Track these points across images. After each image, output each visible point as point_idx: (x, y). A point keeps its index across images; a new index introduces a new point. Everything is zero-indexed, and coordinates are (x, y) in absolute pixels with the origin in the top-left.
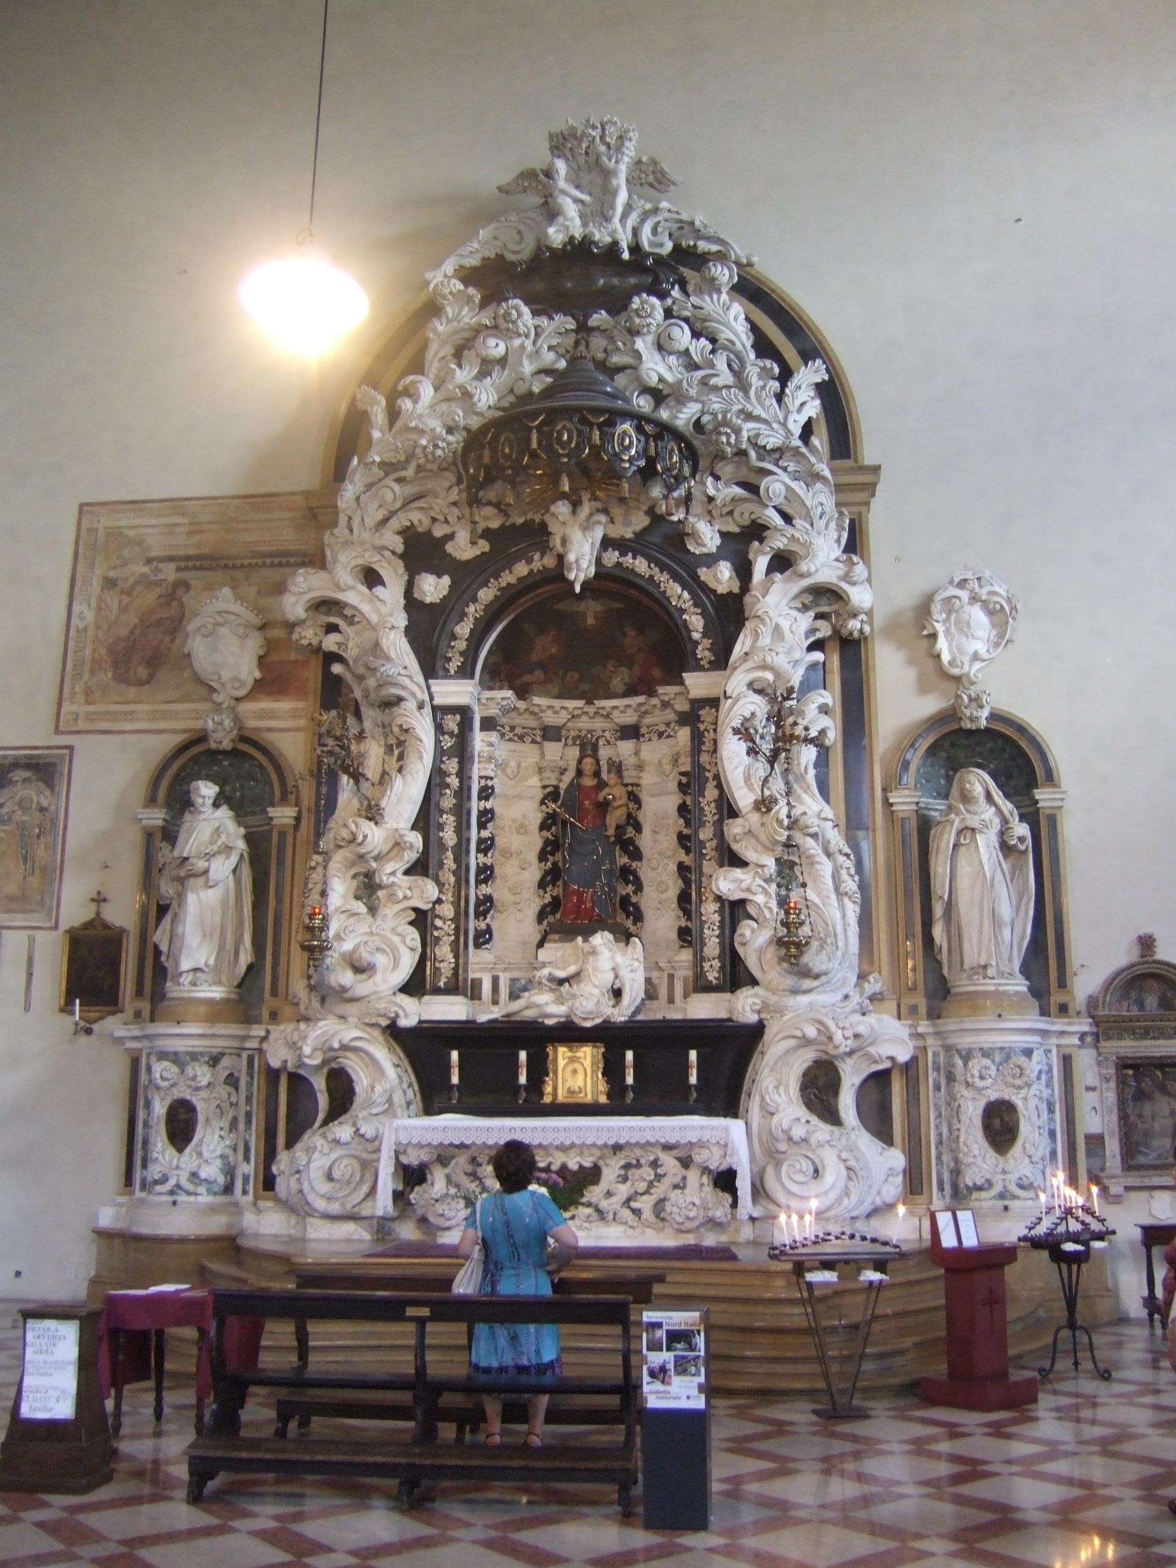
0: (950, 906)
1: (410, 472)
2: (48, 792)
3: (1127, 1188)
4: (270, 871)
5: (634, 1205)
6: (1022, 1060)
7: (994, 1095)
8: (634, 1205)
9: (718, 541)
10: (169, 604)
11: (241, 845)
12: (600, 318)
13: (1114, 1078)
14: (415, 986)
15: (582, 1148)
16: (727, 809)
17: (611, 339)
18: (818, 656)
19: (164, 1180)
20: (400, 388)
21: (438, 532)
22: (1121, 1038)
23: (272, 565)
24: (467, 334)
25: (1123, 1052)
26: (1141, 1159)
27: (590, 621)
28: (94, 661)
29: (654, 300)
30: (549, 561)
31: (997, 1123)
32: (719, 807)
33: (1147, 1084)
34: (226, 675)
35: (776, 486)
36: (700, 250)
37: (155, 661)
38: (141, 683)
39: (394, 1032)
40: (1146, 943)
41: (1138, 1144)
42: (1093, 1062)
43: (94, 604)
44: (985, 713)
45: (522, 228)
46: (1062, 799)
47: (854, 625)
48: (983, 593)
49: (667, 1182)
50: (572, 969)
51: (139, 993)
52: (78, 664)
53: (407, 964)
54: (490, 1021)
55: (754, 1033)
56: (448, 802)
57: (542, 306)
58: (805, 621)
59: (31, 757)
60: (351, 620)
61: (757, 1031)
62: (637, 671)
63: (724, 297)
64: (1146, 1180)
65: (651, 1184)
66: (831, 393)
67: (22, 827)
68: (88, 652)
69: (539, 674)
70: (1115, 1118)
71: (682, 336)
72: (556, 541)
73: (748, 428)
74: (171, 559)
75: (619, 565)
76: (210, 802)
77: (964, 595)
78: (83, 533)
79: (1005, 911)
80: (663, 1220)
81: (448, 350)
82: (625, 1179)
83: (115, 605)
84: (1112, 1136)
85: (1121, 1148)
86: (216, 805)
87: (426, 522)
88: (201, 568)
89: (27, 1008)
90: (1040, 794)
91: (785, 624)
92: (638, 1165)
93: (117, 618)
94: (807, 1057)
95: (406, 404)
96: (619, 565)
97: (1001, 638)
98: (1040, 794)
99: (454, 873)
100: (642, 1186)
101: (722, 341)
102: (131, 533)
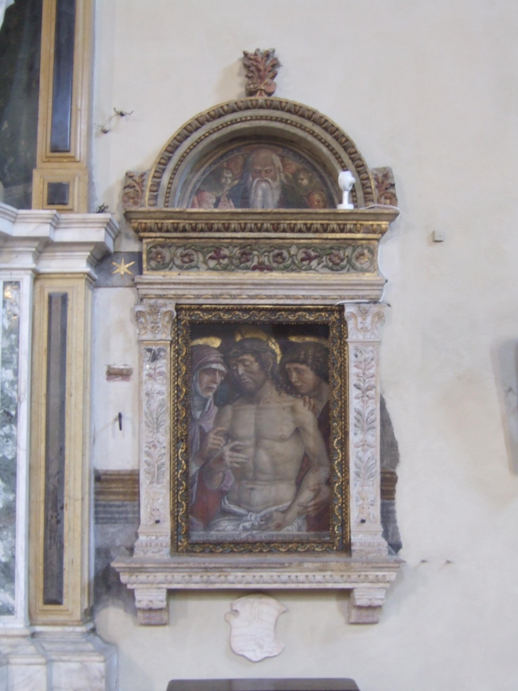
3: (172, 593)
13: (168, 352)
22: (187, 264)
25: (190, 296)
26: (226, 529)
33: (248, 368)
40: (260, 68)
41: (222, 493)
42: (127, 315)
46: (381, 290)
64: (214, 576)
70: (164, 438)
84: (155, 479)
85: (176, 505)
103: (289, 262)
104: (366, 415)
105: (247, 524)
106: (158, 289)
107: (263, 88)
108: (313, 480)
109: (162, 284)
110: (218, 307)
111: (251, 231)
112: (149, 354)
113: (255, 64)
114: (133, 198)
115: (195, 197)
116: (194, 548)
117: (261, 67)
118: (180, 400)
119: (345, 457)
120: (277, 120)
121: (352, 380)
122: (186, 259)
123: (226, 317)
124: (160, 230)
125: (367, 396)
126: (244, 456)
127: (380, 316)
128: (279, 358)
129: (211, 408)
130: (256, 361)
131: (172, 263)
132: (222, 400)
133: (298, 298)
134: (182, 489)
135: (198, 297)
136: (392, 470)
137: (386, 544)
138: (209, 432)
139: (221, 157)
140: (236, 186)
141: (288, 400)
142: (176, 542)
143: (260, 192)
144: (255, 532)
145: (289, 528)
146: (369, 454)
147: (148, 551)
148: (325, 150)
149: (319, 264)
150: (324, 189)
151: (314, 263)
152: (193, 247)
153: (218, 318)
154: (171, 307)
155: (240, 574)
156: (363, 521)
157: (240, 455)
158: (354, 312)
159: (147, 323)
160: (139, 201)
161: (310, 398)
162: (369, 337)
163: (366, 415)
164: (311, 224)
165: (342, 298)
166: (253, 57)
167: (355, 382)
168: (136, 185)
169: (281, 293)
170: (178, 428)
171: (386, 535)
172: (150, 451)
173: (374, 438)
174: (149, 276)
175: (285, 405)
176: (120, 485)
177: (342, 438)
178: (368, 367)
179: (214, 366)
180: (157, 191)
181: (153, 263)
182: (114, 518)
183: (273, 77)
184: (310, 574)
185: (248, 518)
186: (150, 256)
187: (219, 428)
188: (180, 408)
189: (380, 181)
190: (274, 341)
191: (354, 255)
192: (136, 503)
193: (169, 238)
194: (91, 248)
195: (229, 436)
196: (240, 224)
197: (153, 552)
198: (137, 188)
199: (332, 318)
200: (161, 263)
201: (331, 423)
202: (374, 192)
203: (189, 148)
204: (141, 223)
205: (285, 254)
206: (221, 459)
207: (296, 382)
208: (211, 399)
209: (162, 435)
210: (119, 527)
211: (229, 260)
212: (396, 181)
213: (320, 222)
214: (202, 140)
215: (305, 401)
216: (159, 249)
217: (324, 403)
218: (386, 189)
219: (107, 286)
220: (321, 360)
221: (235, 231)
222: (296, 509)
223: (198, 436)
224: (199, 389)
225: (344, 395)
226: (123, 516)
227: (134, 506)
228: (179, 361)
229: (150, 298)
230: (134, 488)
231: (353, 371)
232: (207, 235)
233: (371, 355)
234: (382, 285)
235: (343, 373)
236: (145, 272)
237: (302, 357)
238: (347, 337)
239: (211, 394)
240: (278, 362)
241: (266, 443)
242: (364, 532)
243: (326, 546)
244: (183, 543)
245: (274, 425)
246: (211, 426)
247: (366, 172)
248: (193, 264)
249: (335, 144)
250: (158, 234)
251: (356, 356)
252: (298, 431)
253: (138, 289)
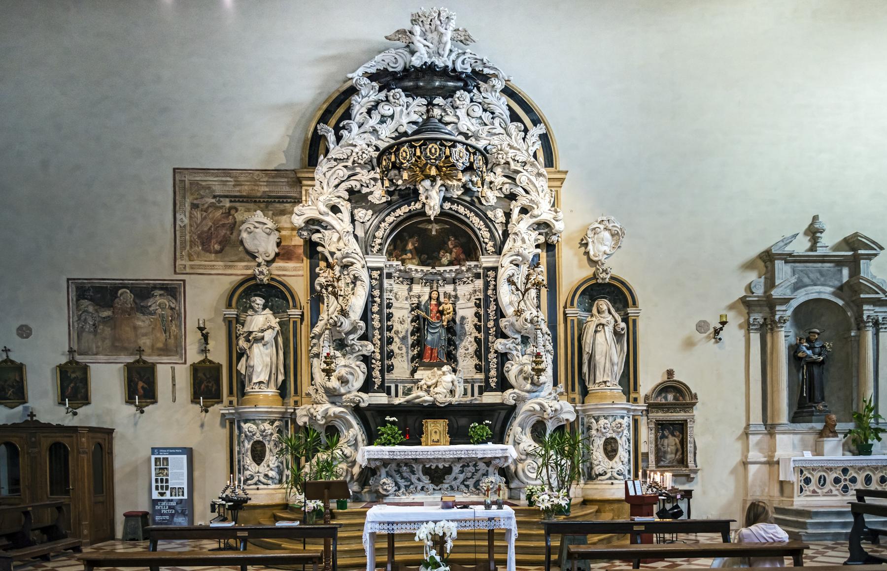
0: (591, 357)
1: (349, 164)
2: (174, 301)
4: (288, 339)
5: (466, 483)
6: (620, 420)
7: (609, 436)
8: (466, 483)
9: (495, 200)
10: (228, 217)
11: (278, 328)
12: (439, 100)
14: (367, 387)
15: (445, 460)
16: (500, 314)
17: (445, 110)
18: (539, 251)
19: (252, 477)
20: (341, 125)
21: (365, 190)
23: (279, 202)
24: (373, 104)
27: (434, 233)
28: (191, 241)
29: (466, 93)
30: (418, 206)
31: (609, 448)
32: (496, 314)
34: (261, 250)
35: (522, 178)
36: (485, 73)
37: (225, 243)
38: (217, 252)
39: (357, 410)
40: (670, 373)
43: (187, 214)
44: (609, 276)
45: (397, 56)
47: (554, 238)
48: (610, 226)
49: (480, 473)
50: (434, 381)
51: (231, 393)
52: (183, 243)
53: (362, 378)
54: (400, 404)
55: (510, 411)
56: (376, 308)
57: (411, 92)
58: (535, 234)
59: (163, 284)
60: (325, 228)
61: (513, 408)
62: (454, 255)
63: (498, 94)
65: (473, 474)
66: (545, 139)
67: (162, 316)
68: (188, 237)
69: (409, 255)
70: (653, 446)
71: (478, 111)
72: (422, 198)
73: (511, 153)
74: (226, 197)
75: (451, 209)
76: (261, 307)
77: (602, 227)
78: (177, 182)
79: (615, 359)
80: (478, 489)
81: (364, 110)
82: (462, 472)
83: (199, 216)
86: (264, 309)
87: (359, 186)
88: (243, 202)
89: (174, 400)
90: (630, 310)
91: (526, 238)
92: (468, 466)
93: (202, 222)
94: (534, 419)
95: (344, 133)
96: (451, 209)
97: (617, 246)
98: (630, 310)
99: (380, 340)
100: (469, 475)
101: (497, 114)
102: (204, 183)
108: (679, 453)
173: (692, 445)
242: (691, 464)
245: (671, 443)
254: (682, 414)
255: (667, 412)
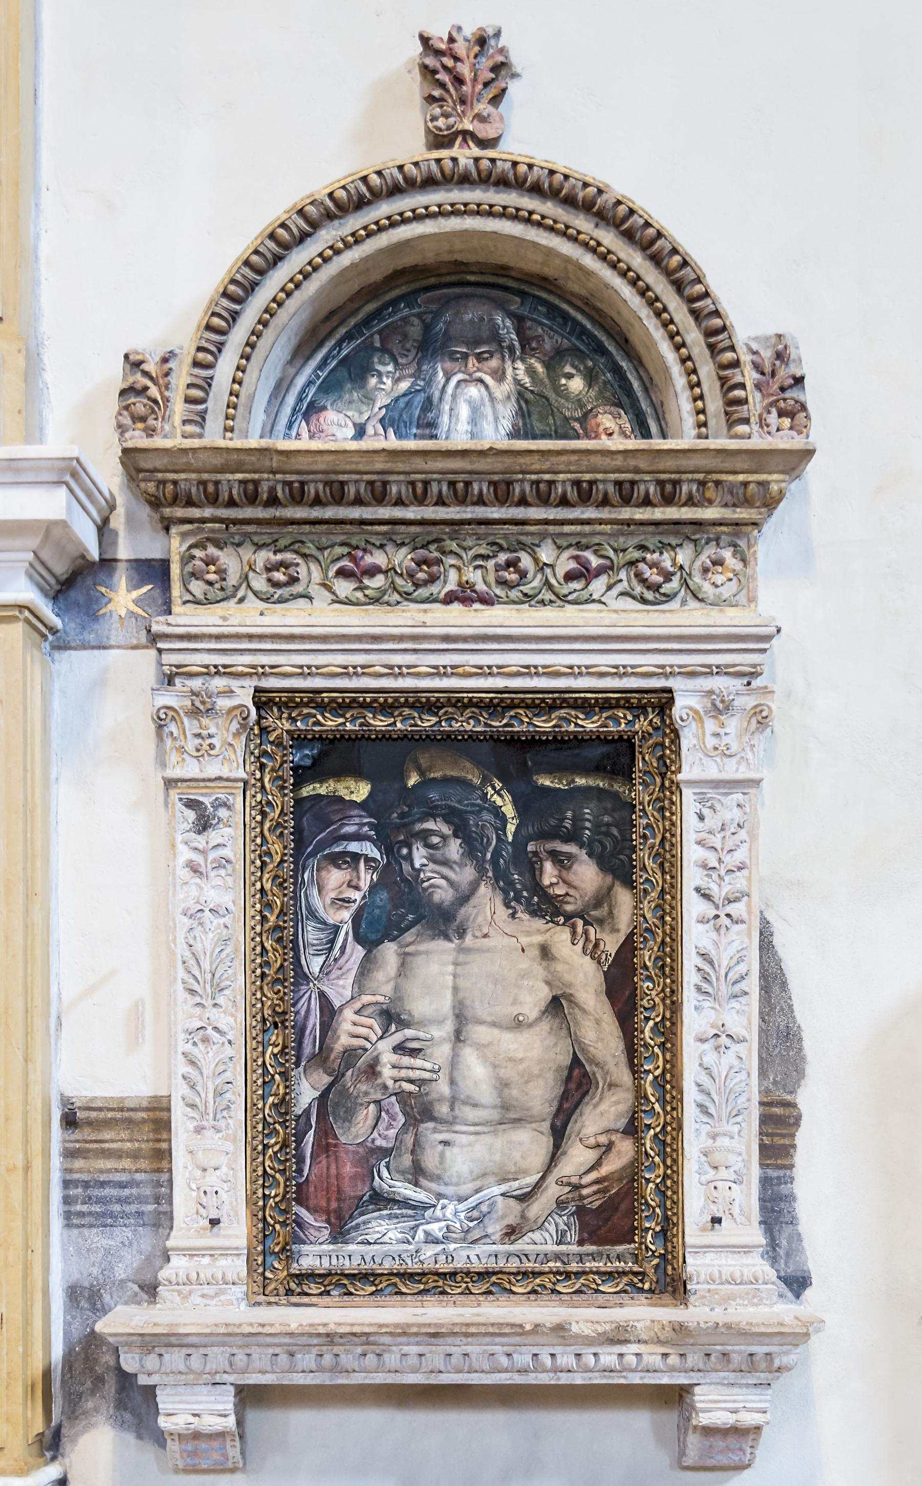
3: (250, 1397)
25: (291, 670)
40: (460, 74)
70: (231, 1017)
103: (536, 583)
104: (724, 964)
105: (436, 1228)
106: (209, 651)
107: (470, 128)
108: (601, 1115)
109: (218, 637)
110: (361, 697)
111: (441, 502)
112: (191, 815)
113: (449, 63)
114: (143, 419)
115: (303, 423)
116: (303, 1284)
117: (465, 70)
118: (267, 926)
119: (673, 1066)
120: (504, 214)
121: (692, 877)
122: (279, 576)
123: (380, 723)
124: (213, 500)
125: (728, 915)
126: (428, 1065)
127: (761, 719)
128: (511, 828)
129: (348, 950)
130: (456, 836)
131: (244, 585)
132: (373, 930)
133: (558, 675)
134: (276, 1143)
135: (305, 672)
136: (788, 1097)
137: (772, 1274)
138: (342, 1008)
139: (366, 322)
140: (404, 395)
141: (534, 930)
142: (261, 1270)
143: (464, 411)
144: (452, 1246)
145: (536, 1236)
146: (729, 1058)
147: (190, 1293)
148: (627, 291)
149: (610, 588)
150: (625, 400)
151: (598, 586)
152: (296, 546)
153: (361, 725)
154: (245, 697)
155: (414, 1350)
156: (716, 1221)
157: (418, 1063)
158: (699, 707)
159: (186, 737)
160: (158, 424)
161: (586, 923)
162: (732, 770)
163: (724, 964)
164: (591, 483)
165: (664, 672)
166: (443, 46)
167: (698, 882)
168: (149, 383)
169: (515, 660)
170: (263, 995)
171: (772, 1251)
172: (195, 1051)
173: (744, 1018)
174: (186, 617)
175: (524, 940)
176: (124, 1135)
177: (664, 1017)
178: (729, 844)
179: (354, 847)
180: (203, 401)
181: (197, 587)
182: (112, 1215)
183: (496, 100)
184: (588, 1351)
185: (438, 1213)
186: (189, 568)
187: (366, 999)
188: (268, 945)
189: (768, 369)
190: (498, 785)
191: (698, 564)
192: (165, 1177)
193: (235, 522)
194: (34, 542)
195: (391, 1017)
196: (413, 483)
197: (203, 1296)
198: (154, 391)
199: (641, 725)
200: (217, 586)
201: (639, 985)
202: (750, 400)
203: (283, 290)
204: (164, 482)
205: (526, 561)
206: (372, 1070)
207: (552, 884)
208: (347, 928)
209: (225, 1012)
210: (123, 1234)
211: (387, 577)
212: (806, 370)
213: (613, 476)
214: (316, 269)
215: (574, 933)
216: (212, 550)
217: (622, 938)
218: (783, 389)
219: (85, 646)
220: (615, 831)
221: (399, 502)
222: (552, 1191)
223: (315, 1020)
224: (317, 903)
225: (670, 914)
226: (133, 1208)
227: (159, 1185)
228: (266, 833)
229: (191, 675)
230: (159, 1141)
231: (692, 854)
232: (329, 513)
233: (737, 814)
234: (768, 638)
235: (668, 858)
236: (176, 609)
237: (568, 824)
238: (679, 770)
239: (346, 915)
240: (510, 839)
241: (480, 1033)
242: (720, 1250)
243: (625, 1280)
244: (279, 1270)
245: (484, 996)
246: (348, 994)
247: (732, 348)
248: (298, 589)
249: (652, 276)
250: (208, 512)
251: (701, 818)
252: (558, 1006)
253: (160, 651)
254: (610, 611)
255: (417, 585)
